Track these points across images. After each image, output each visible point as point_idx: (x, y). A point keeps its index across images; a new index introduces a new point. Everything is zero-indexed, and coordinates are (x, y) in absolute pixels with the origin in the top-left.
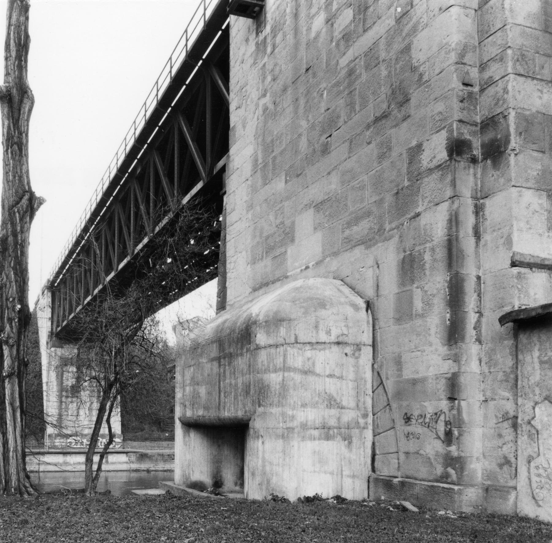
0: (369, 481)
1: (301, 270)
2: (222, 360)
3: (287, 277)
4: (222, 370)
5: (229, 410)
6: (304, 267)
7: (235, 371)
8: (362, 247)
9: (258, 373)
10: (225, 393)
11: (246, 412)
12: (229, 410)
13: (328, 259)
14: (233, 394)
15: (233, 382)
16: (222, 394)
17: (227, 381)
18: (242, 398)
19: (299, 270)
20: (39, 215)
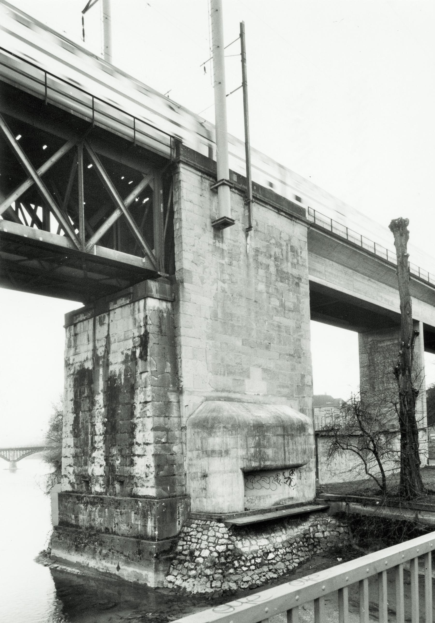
0: (221, 513)
1: (255, 394)
2: (286, 437)
3: (134, 384)
4: (286, 441)
5: (293, 461)
6: (256, 394)
7: (296, 442)
8: (286, 398)
9: (310, 445)
10: (289, 453)
11: (304, 461)
12: (293, 461)
13: (270, 396)
14: (295, 453)
15: (295, 448)
16: (287, 454)
17: (291, 447)
18: (301, 455)
19: (253, 394)
20: (394, 243)
